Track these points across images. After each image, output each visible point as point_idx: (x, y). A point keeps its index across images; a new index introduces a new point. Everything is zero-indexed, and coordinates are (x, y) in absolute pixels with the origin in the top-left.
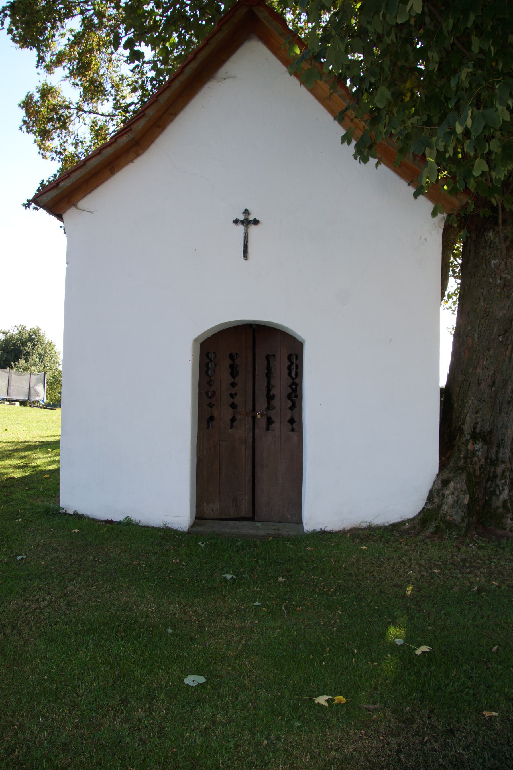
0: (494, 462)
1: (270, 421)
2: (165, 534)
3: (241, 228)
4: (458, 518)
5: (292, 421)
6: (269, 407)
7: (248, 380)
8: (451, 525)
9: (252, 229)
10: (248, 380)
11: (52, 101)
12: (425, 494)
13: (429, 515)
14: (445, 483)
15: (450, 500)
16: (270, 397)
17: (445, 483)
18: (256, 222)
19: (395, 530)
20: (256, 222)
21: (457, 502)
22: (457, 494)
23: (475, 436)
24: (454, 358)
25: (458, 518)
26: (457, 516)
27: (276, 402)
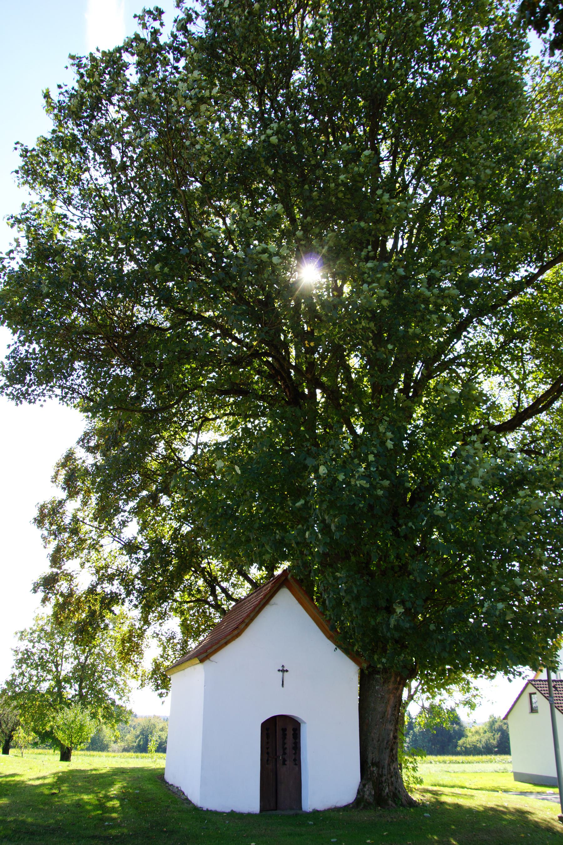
0: (381, 776)
1: (284, 761)
2: (250, 815)
3: (281, 673)
4: (371, 800)
5: (295, 760)
6: (284, 753)
7: (281, 738)
8: (369, 804)
9: (285, 673)
10: (281, 738)
11: (481, 731)
12: (356, 791)
13: (360, 801)
14: (364, 785)
15: (368, 793)
16: (284, 749)
17: (364, 785)
18: (287, 671)
19: (346, 808)
20: (287, 671)
21: (370, 793)
22: (369, 791)
23: (373, 764)
24: (146, 774)
25: (371, 800)
26: (371, 800)
27: (288, 751)
